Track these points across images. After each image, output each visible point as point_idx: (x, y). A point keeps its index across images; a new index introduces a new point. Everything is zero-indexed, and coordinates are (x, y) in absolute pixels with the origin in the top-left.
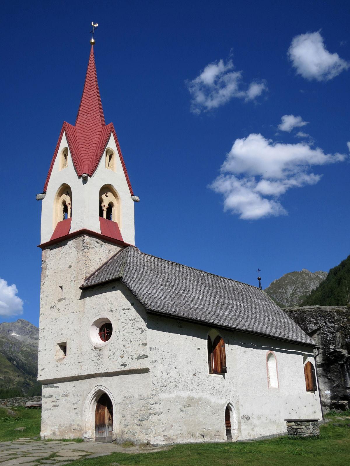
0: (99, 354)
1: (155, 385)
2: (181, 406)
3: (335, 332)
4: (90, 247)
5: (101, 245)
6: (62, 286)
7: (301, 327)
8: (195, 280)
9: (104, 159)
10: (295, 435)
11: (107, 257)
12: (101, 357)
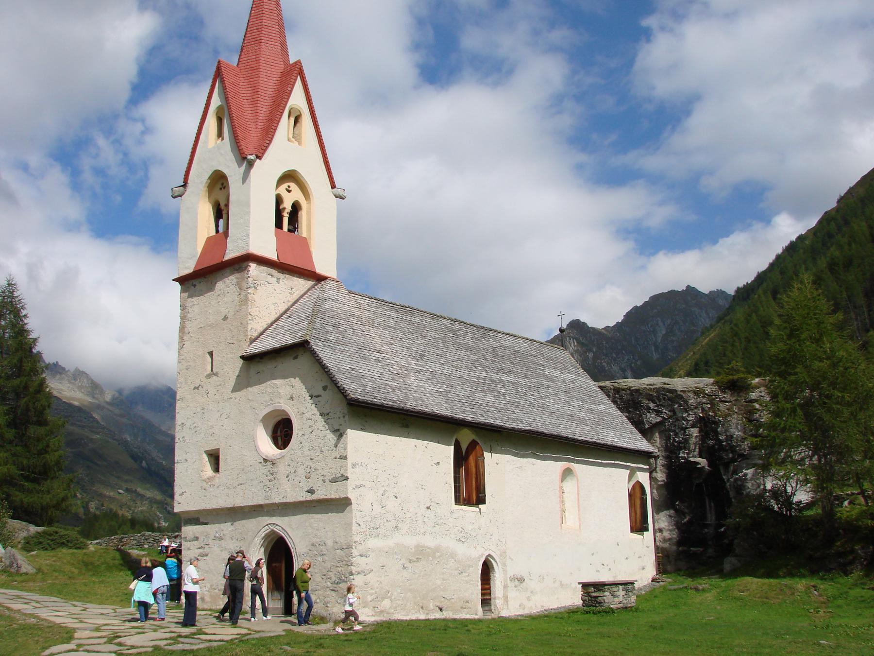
0: (271, 472)
1: (359, 525)
2: (403, 561)
3: (689, 428)
4: (258, 284)
5: (278, 279)
6: (212, 352)
7: (629, 419)
8: (441, 339)
9: (285, 124)
10: (593, 606)
11: (288, 301)
12: (274, 476)
